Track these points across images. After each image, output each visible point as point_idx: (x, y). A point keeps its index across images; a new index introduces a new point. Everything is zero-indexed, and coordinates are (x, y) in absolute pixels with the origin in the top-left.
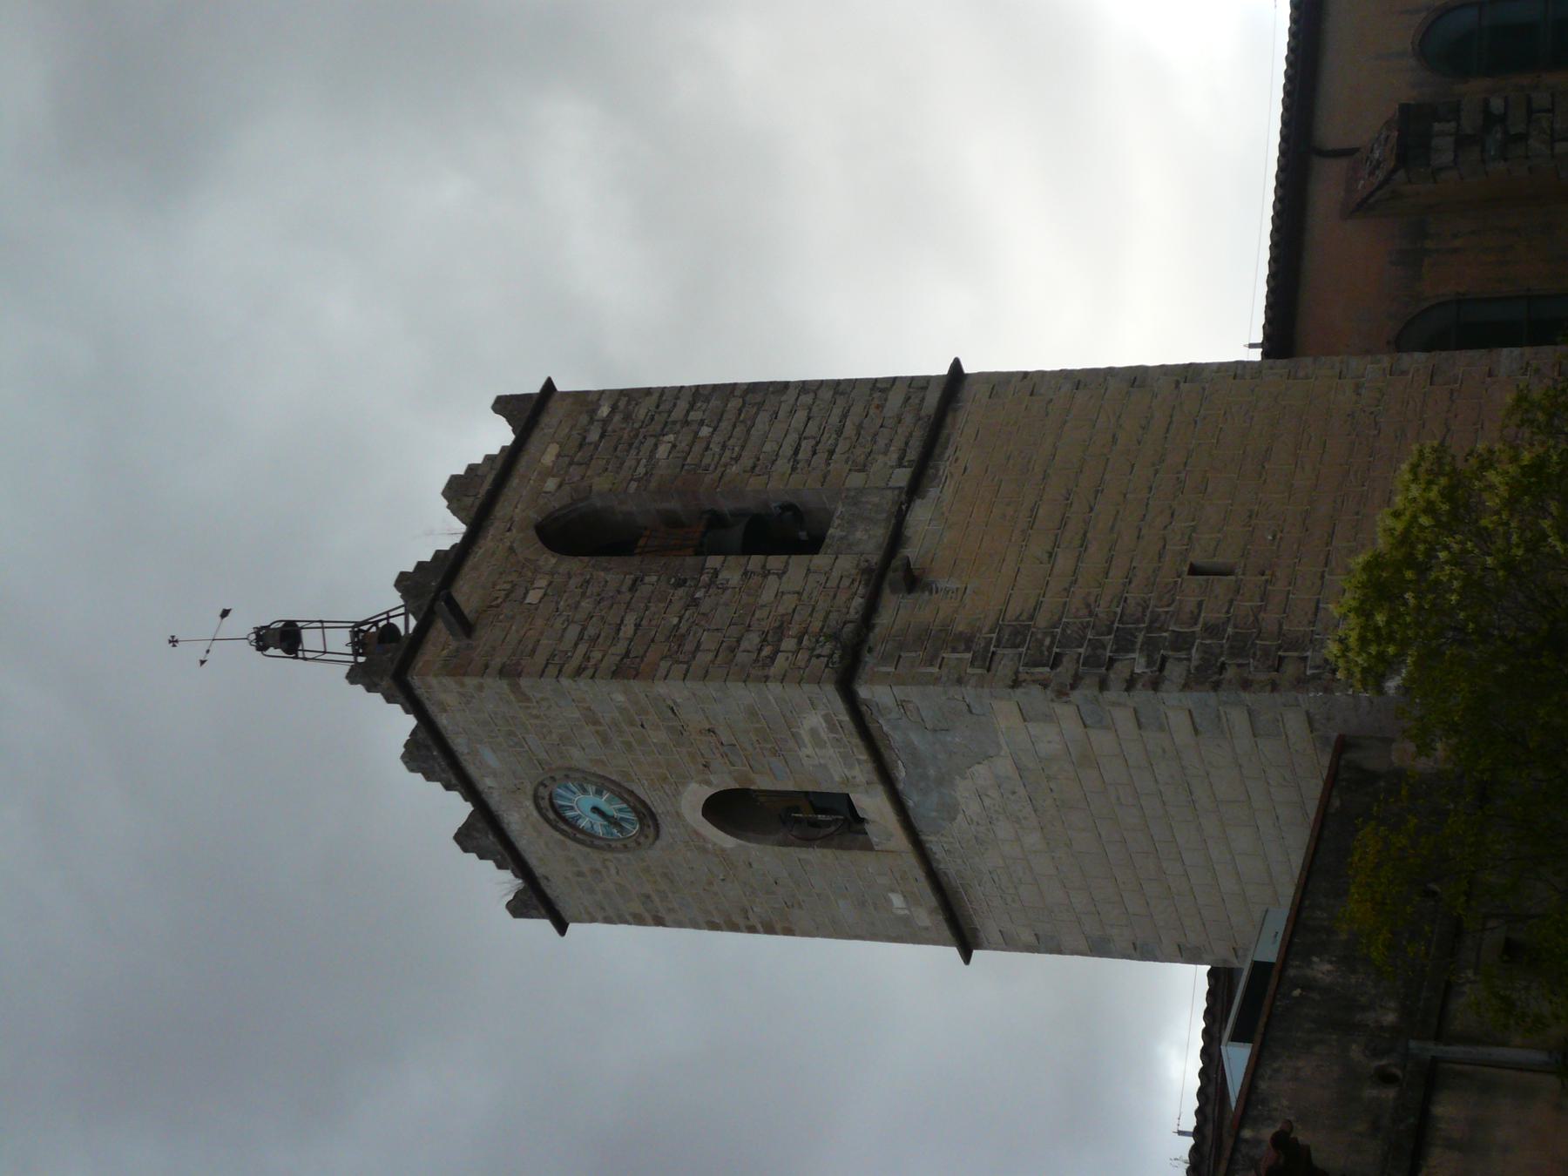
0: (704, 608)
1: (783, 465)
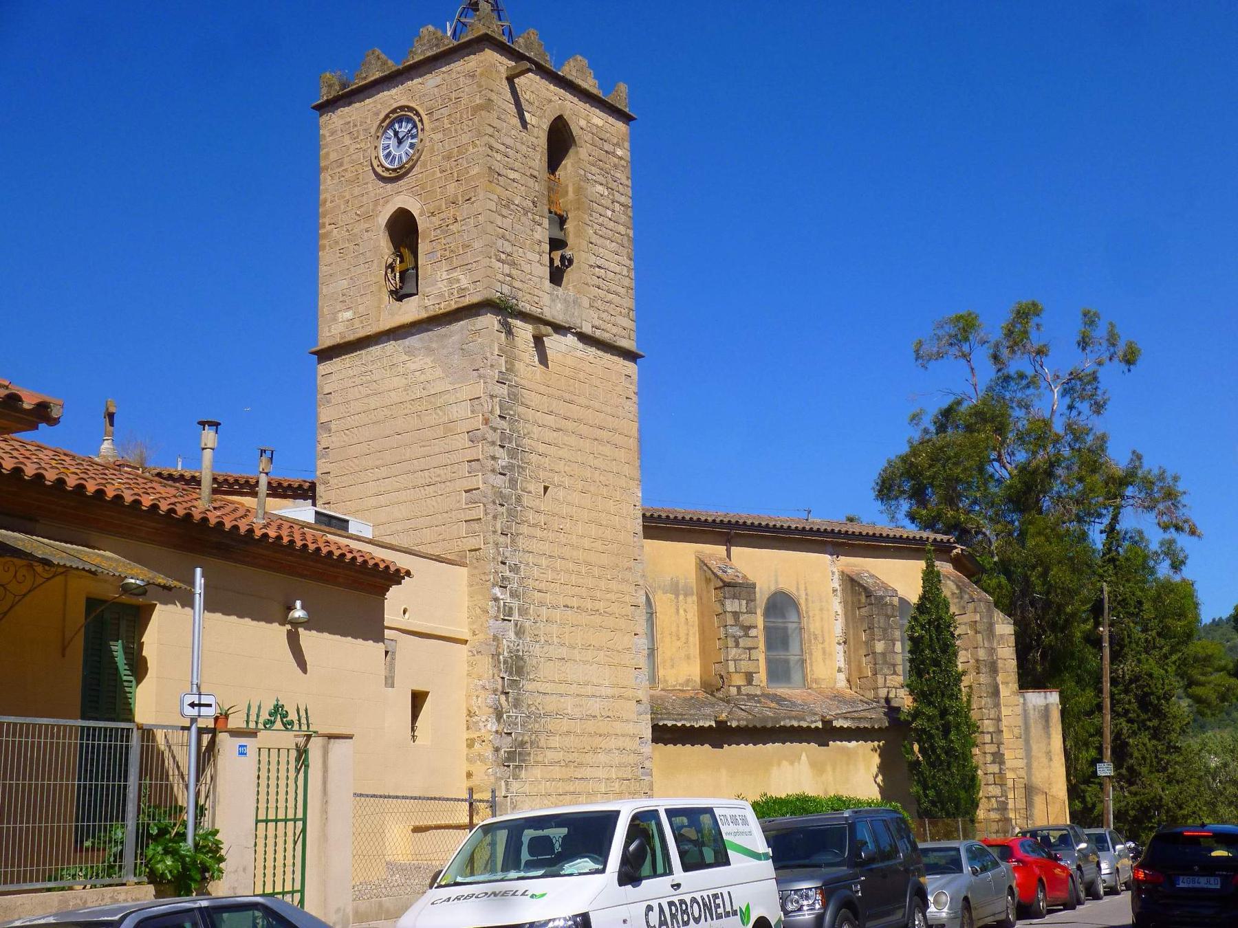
0: (523, 219)
1: (593, 260)
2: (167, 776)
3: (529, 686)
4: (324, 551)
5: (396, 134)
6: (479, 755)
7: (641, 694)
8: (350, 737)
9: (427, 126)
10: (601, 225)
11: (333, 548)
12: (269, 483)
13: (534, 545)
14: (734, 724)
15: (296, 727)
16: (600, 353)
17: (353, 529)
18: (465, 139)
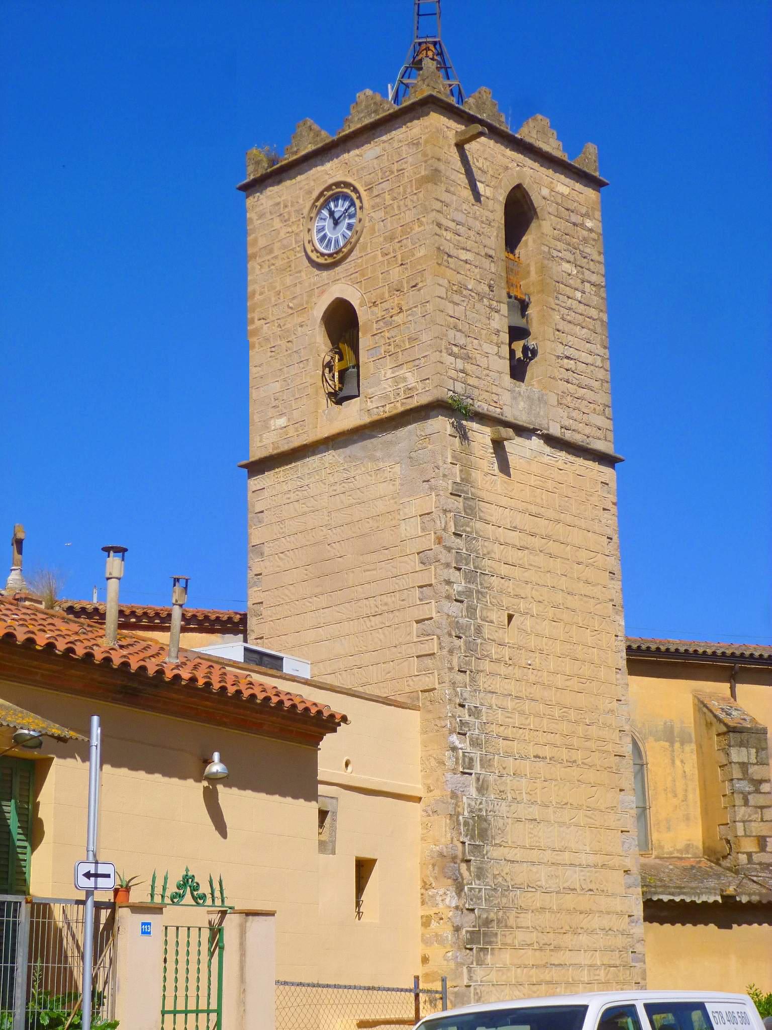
0: (478, 306)
2: (66, 957)
3: (495, 853)
4: (246, 694)
5: (332, 213)
6: (437, 935)
7: (629, 863)
8: (271, 914)
9: (366, 204)
10: (570, 309)
11: (257, 691)
12: (183, 615)
13: (498, 684)
14: (744, 899)
15: (209, 901)
16: (571, 458)
17: (288, 667)
18: (409, 216)
